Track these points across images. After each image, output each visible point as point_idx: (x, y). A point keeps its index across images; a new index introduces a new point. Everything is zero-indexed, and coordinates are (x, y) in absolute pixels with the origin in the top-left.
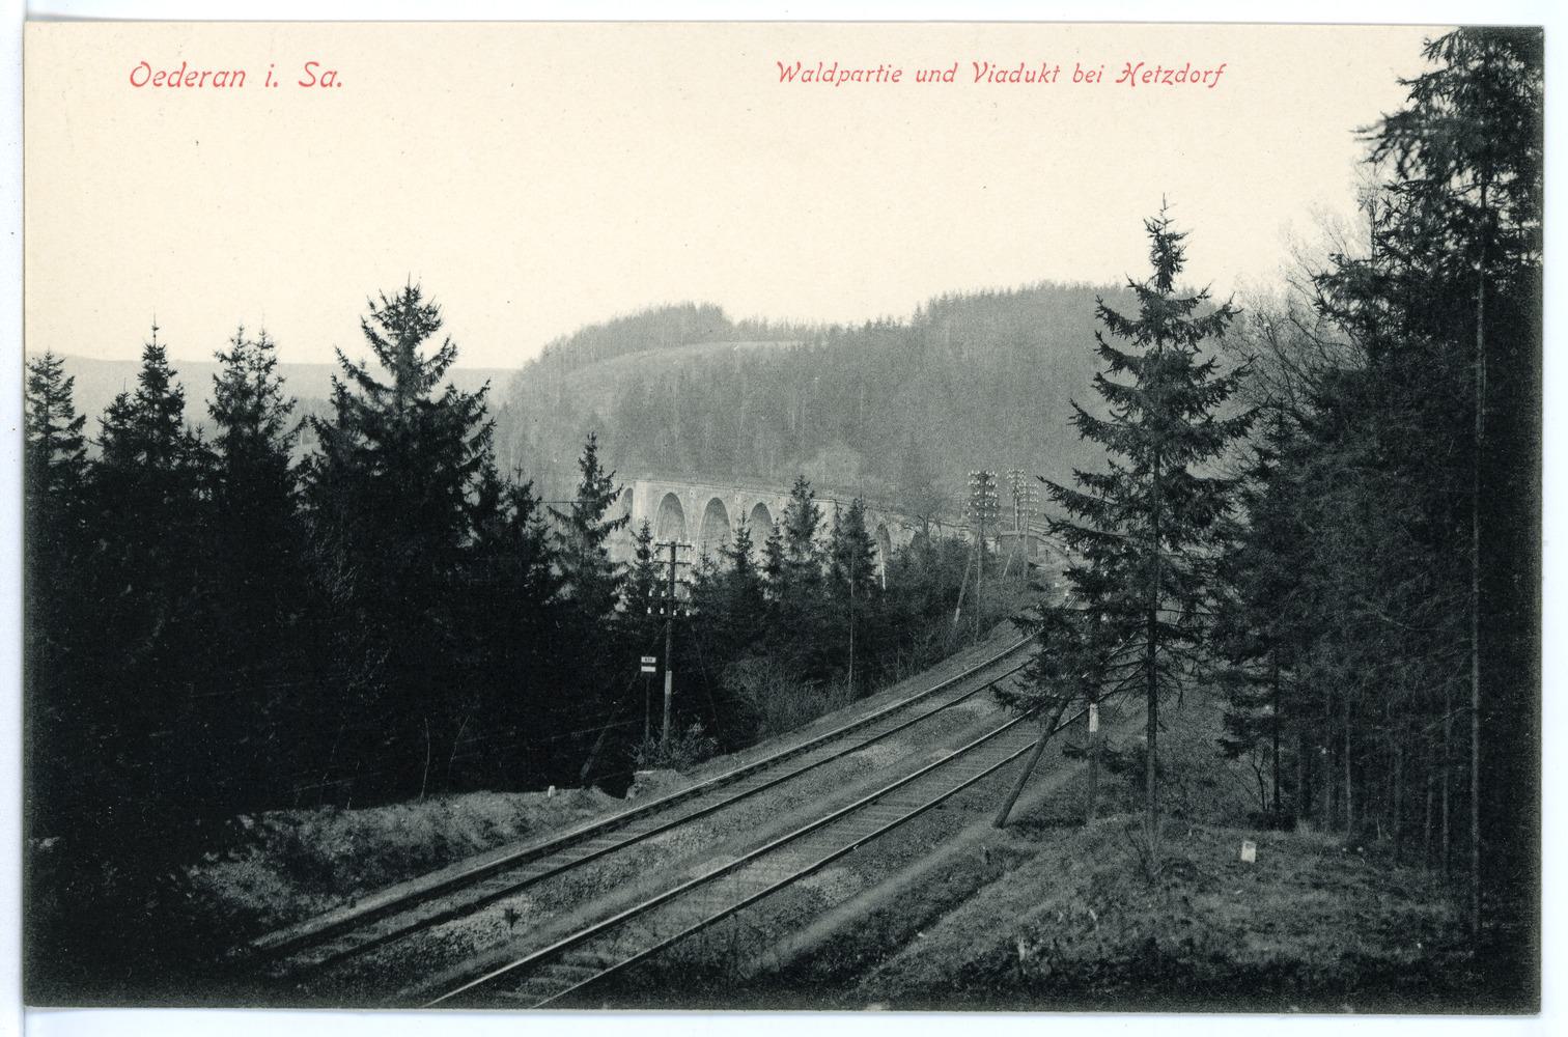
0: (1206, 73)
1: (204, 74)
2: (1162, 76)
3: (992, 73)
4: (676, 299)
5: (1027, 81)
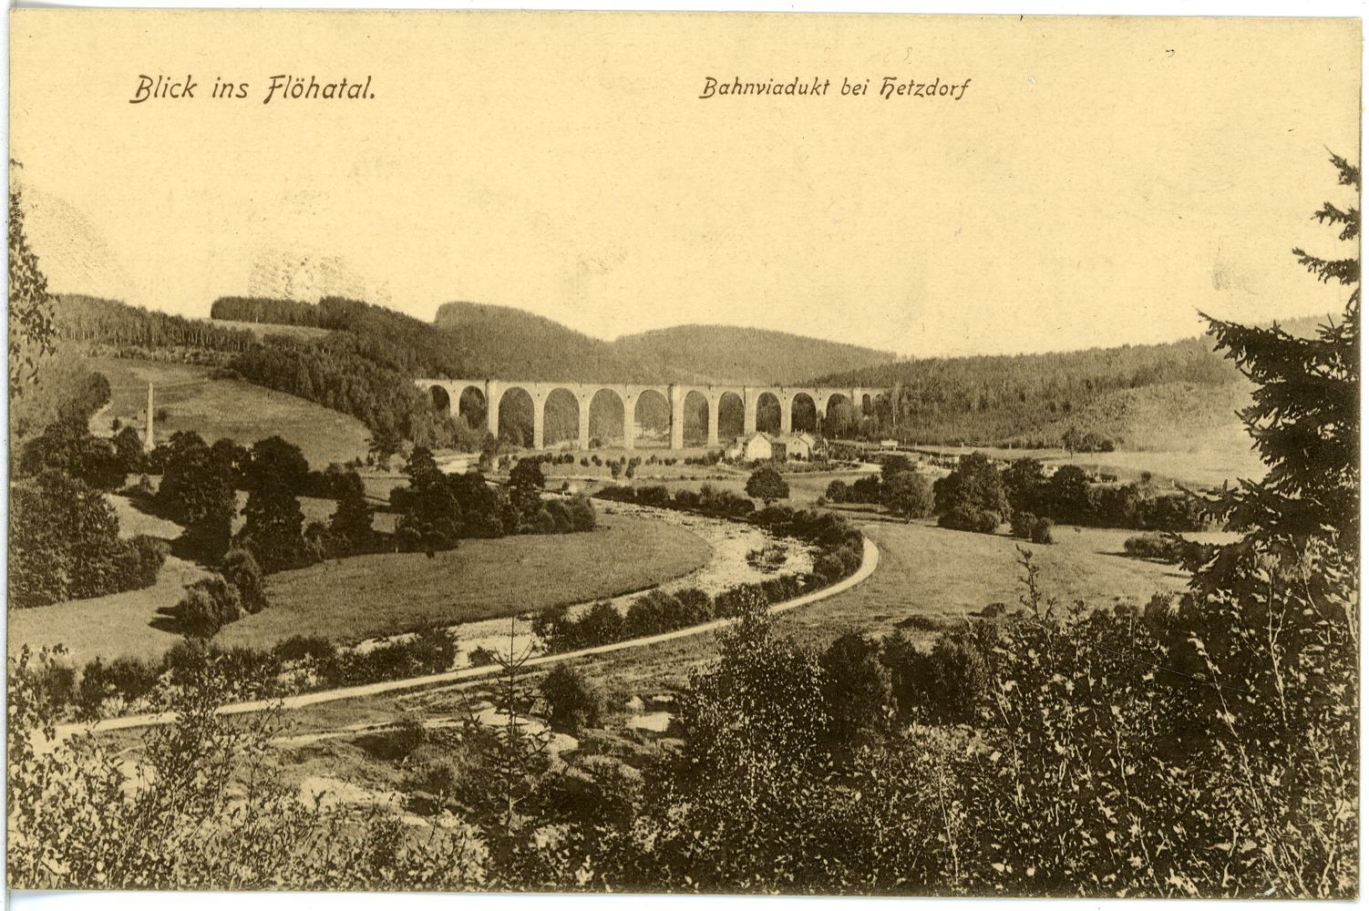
0: (953, 87)
1: (953, 87)
2: (914, 89)
3: (166, 85)
5: (350, 97)
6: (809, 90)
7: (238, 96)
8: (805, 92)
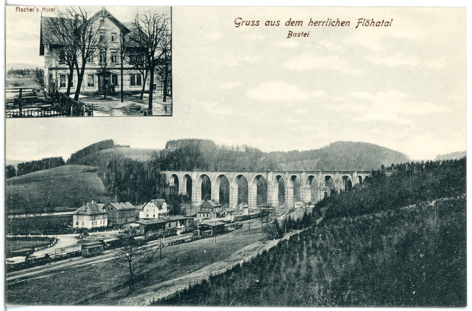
1: (320, 22)
3: (330, 22)
4: (455, 151)
5: (385, 26)
7: (251, 25)
8: (347, 22)
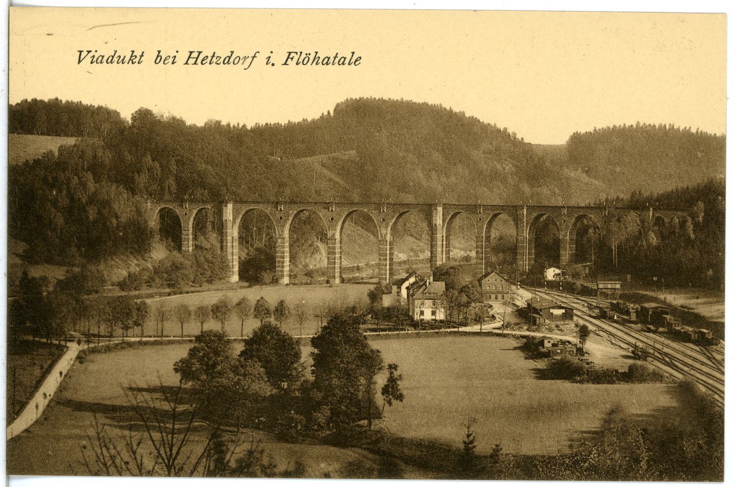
6: (127, 59)
